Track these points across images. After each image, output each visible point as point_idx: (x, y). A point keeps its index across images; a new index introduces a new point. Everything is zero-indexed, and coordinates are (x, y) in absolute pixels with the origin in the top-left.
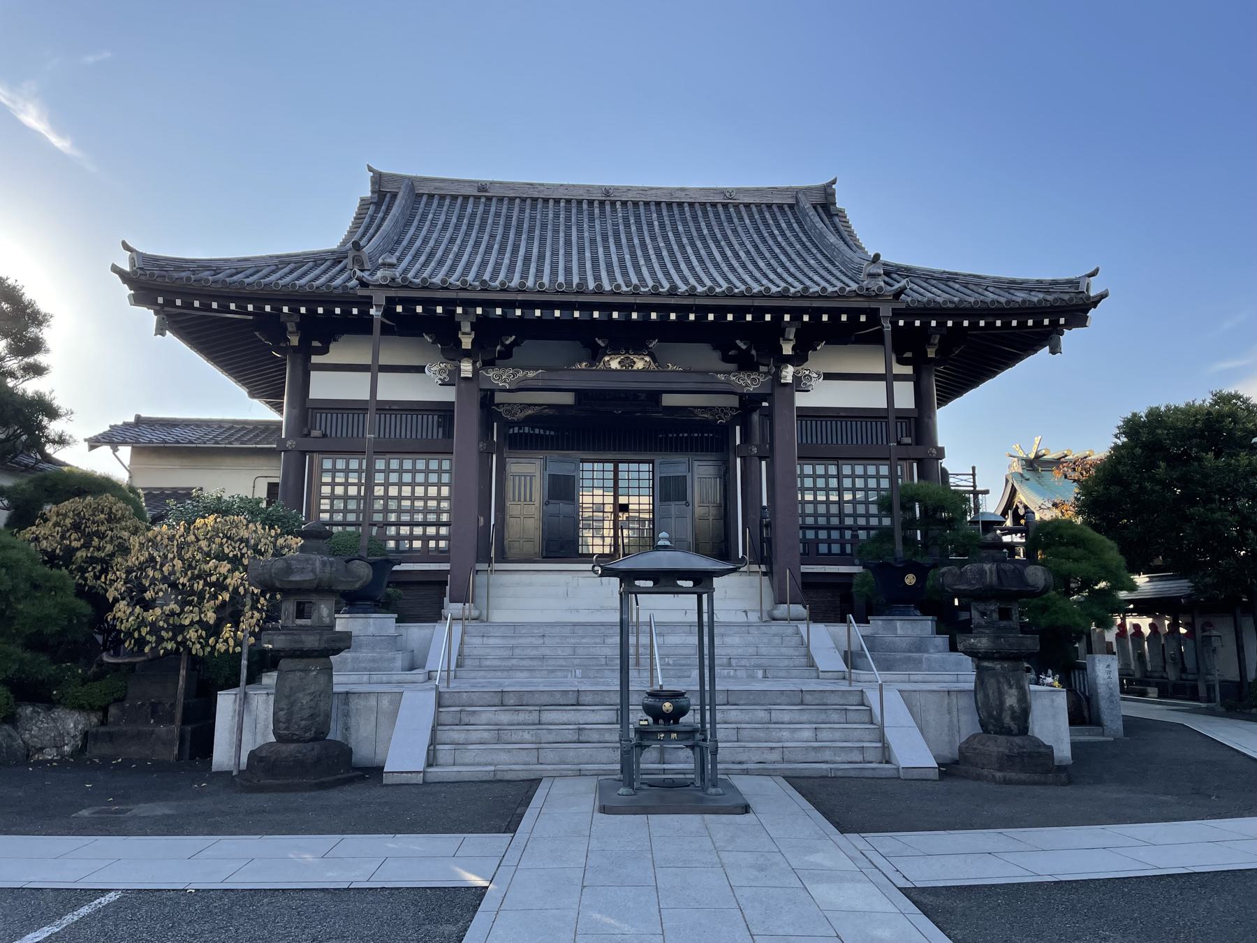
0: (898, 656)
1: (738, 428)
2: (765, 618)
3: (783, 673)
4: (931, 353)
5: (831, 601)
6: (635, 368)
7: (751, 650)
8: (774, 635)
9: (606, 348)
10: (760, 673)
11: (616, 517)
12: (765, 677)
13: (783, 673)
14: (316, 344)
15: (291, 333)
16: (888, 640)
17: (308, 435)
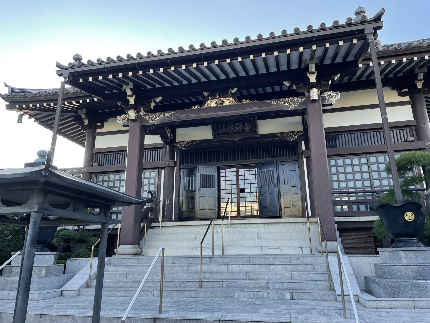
0: (403, 283)
1: (303, 142)
2: (314, 251)
3: (306, 296)
4: (420, 85)
5: (357, 238)
6: (225, 104)
7: (287, 276)
8: (307, 264)
9: (208, 96)
10: (288, 296)
11: (238, 195)
12: (292, 299)
13: (306, 296)
14: (99, 124)
15: (84, 119)
16: (394, 268)
17: (92, 165)
